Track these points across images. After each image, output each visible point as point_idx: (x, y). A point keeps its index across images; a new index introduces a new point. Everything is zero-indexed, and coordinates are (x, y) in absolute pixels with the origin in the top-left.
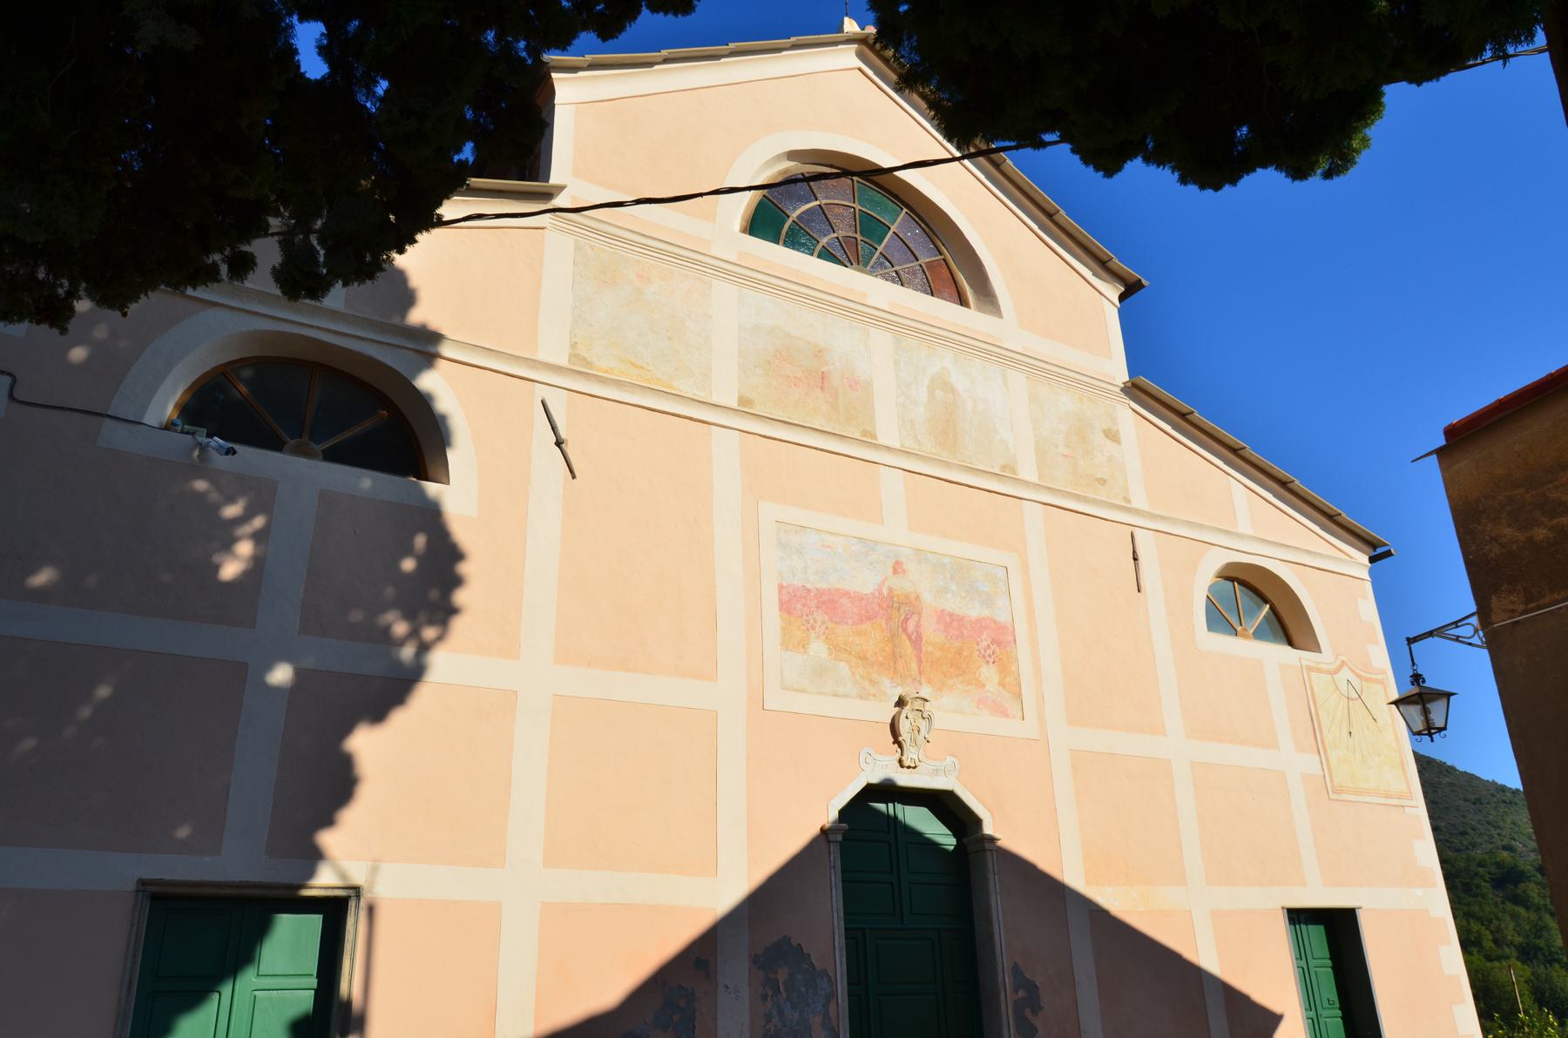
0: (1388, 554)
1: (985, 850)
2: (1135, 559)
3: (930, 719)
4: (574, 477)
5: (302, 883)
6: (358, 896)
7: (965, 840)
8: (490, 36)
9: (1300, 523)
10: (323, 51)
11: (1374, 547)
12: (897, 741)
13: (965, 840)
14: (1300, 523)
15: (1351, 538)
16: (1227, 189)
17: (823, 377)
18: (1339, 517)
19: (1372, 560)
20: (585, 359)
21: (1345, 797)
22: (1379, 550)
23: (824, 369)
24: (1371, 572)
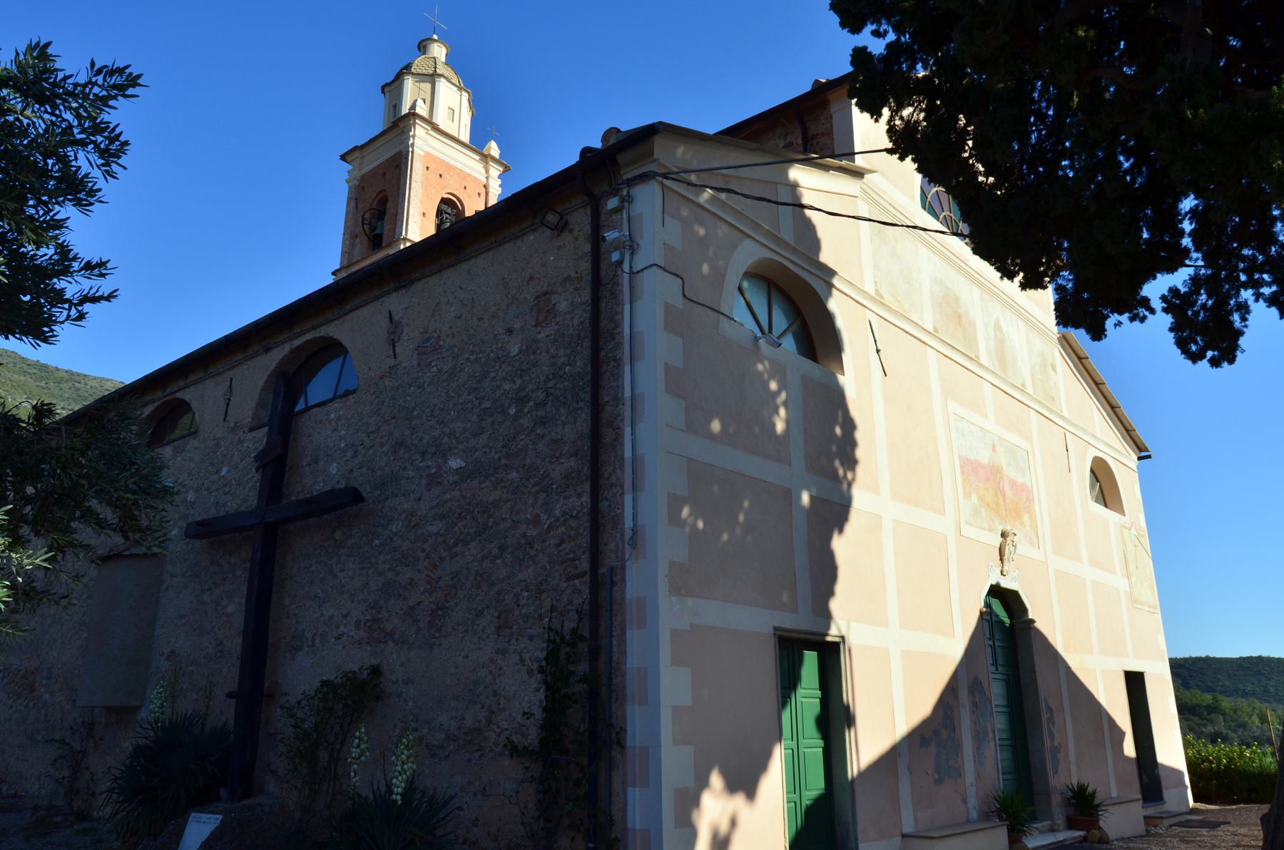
0: (1149, 457)
1: (1031, 628)
2: (1067, 451)
3: (1015, 547)
4: (886, 375)
5: (824, 632)
6: (844, 642)
7: (1014, 621)
8: (1227, 287)
9: (1025, 404)
10: (983, 167)
11: (1140, 450)
12: (1001, 559)
13: (1014, 621)
14: (1025, 404)
15: (1133, 445)
16: (850, 58)
17: (960, 317)
18: (1133, 432)
19: (1140, 458)
20: (880, 294)
21: (1138, 606)
22: (1143, 454)
23: (960, 311)
24: (1138, 467)
